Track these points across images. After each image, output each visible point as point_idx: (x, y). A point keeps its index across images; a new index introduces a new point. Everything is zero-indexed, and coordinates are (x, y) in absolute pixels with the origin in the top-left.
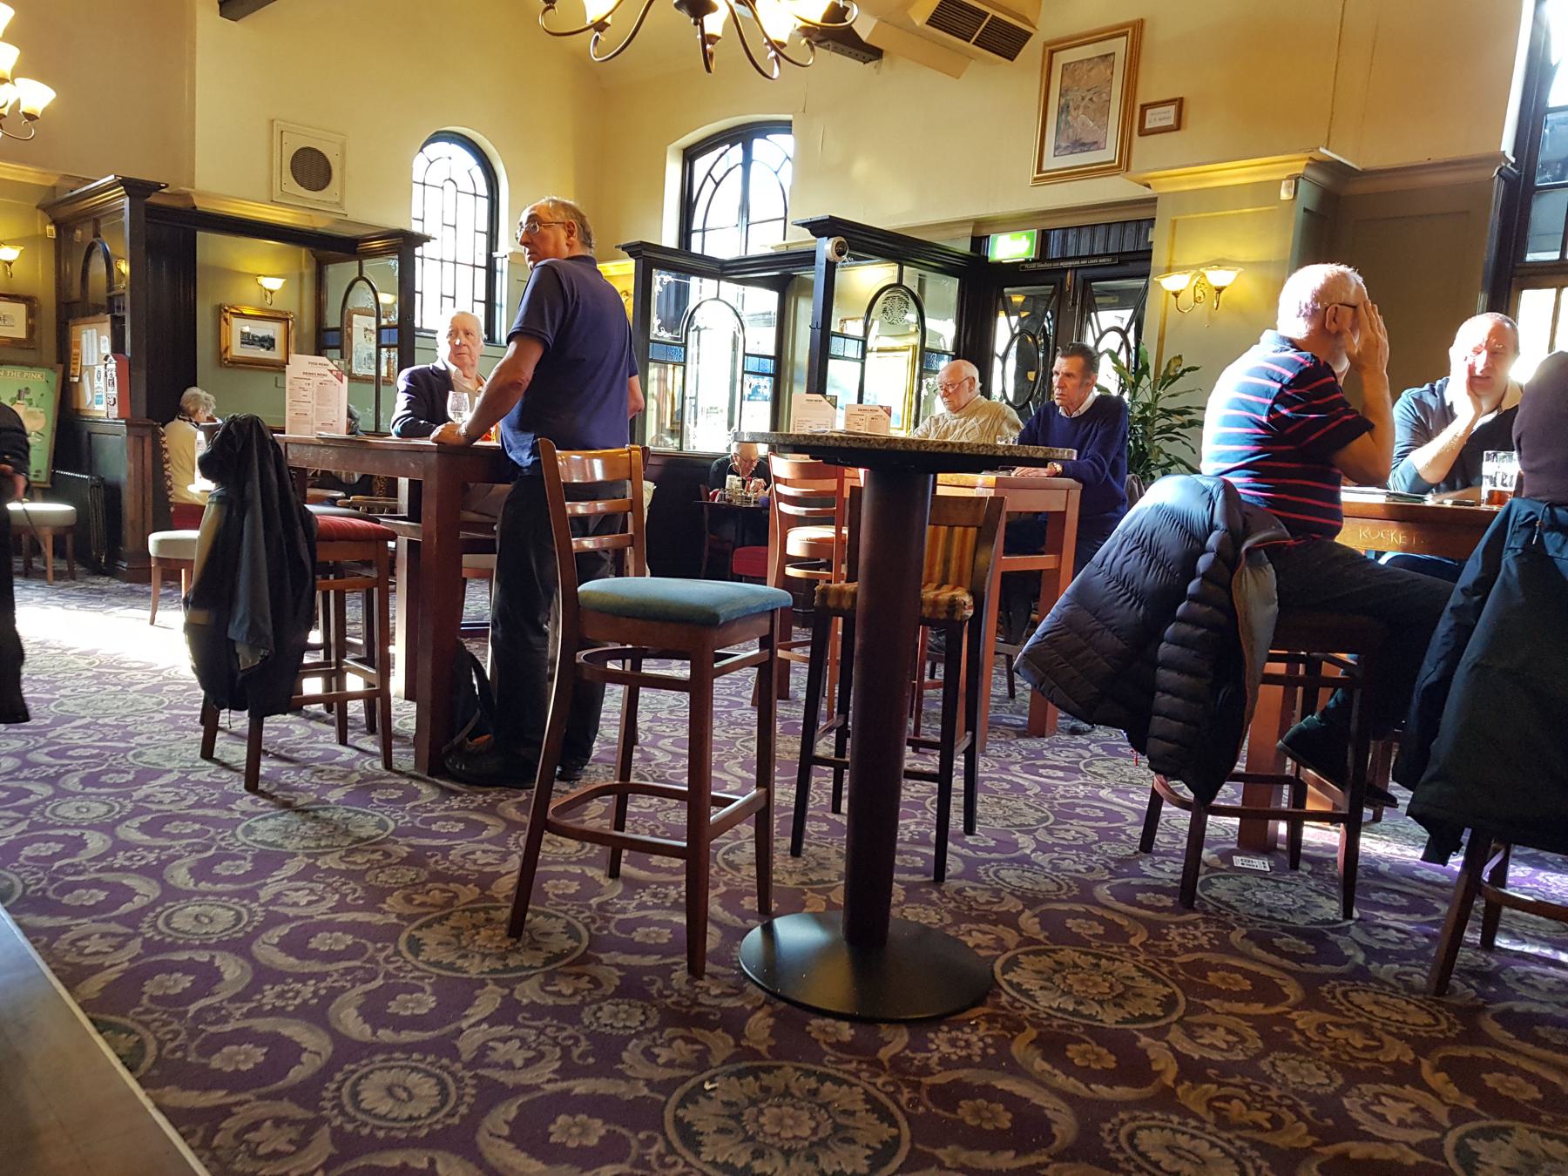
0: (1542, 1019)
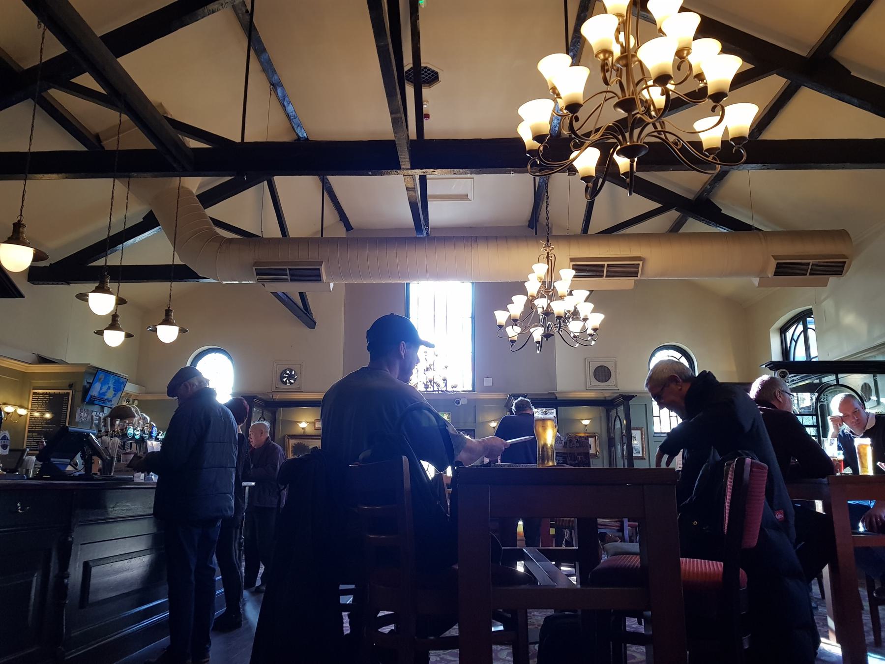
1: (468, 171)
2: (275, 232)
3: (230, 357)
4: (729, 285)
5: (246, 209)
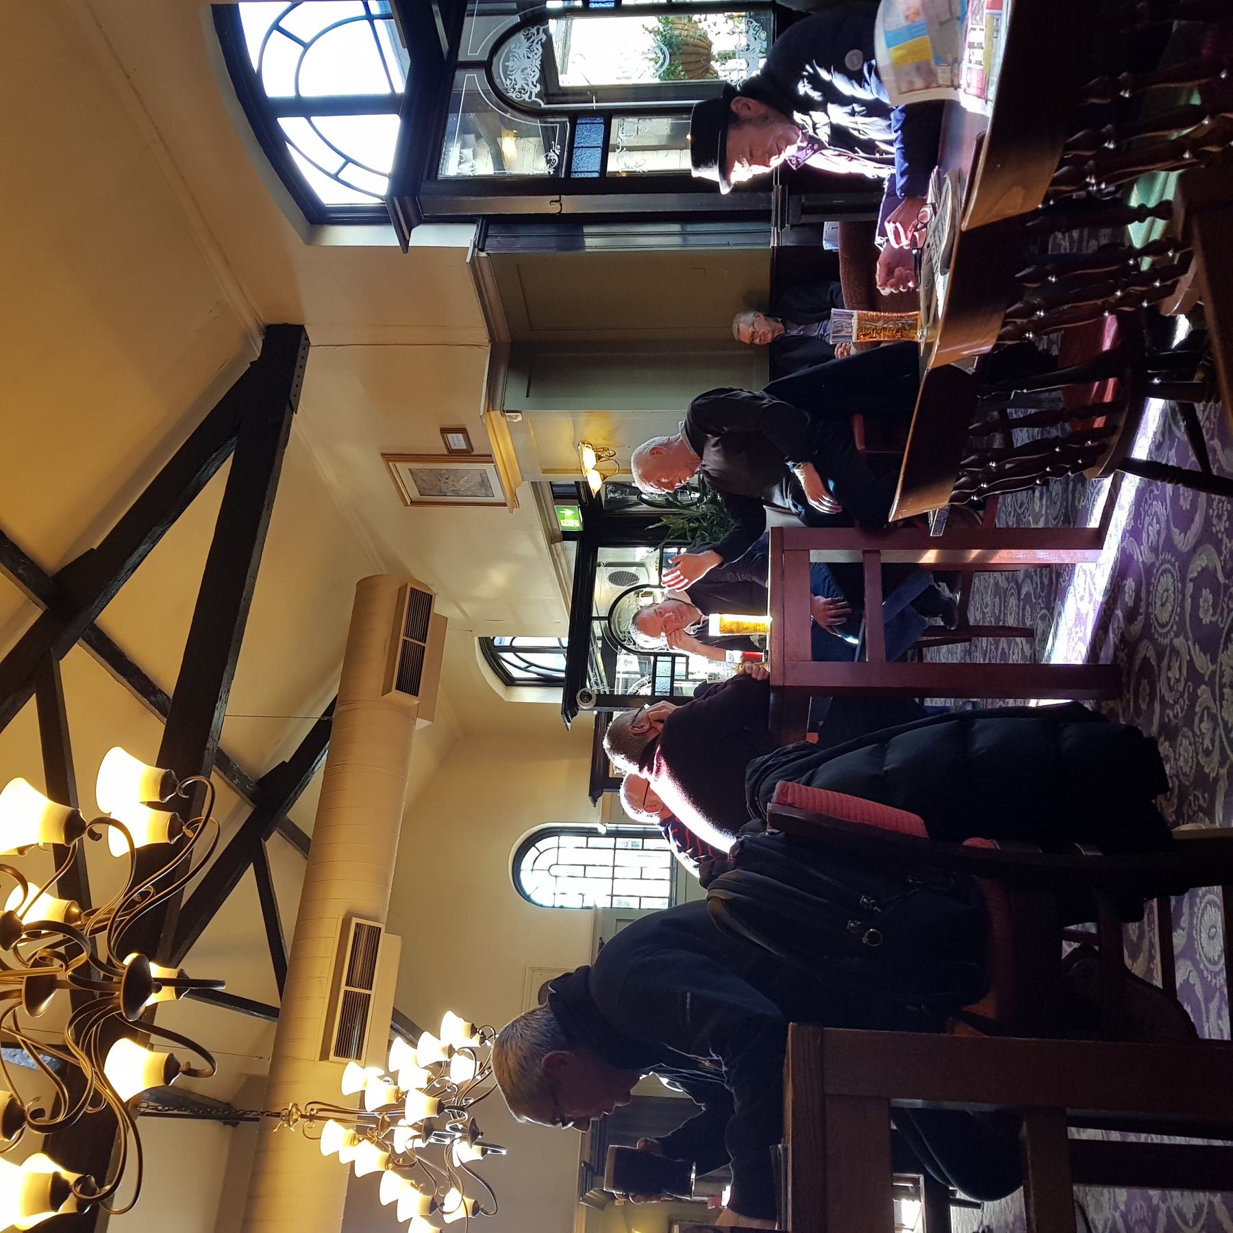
4: (421, 757)
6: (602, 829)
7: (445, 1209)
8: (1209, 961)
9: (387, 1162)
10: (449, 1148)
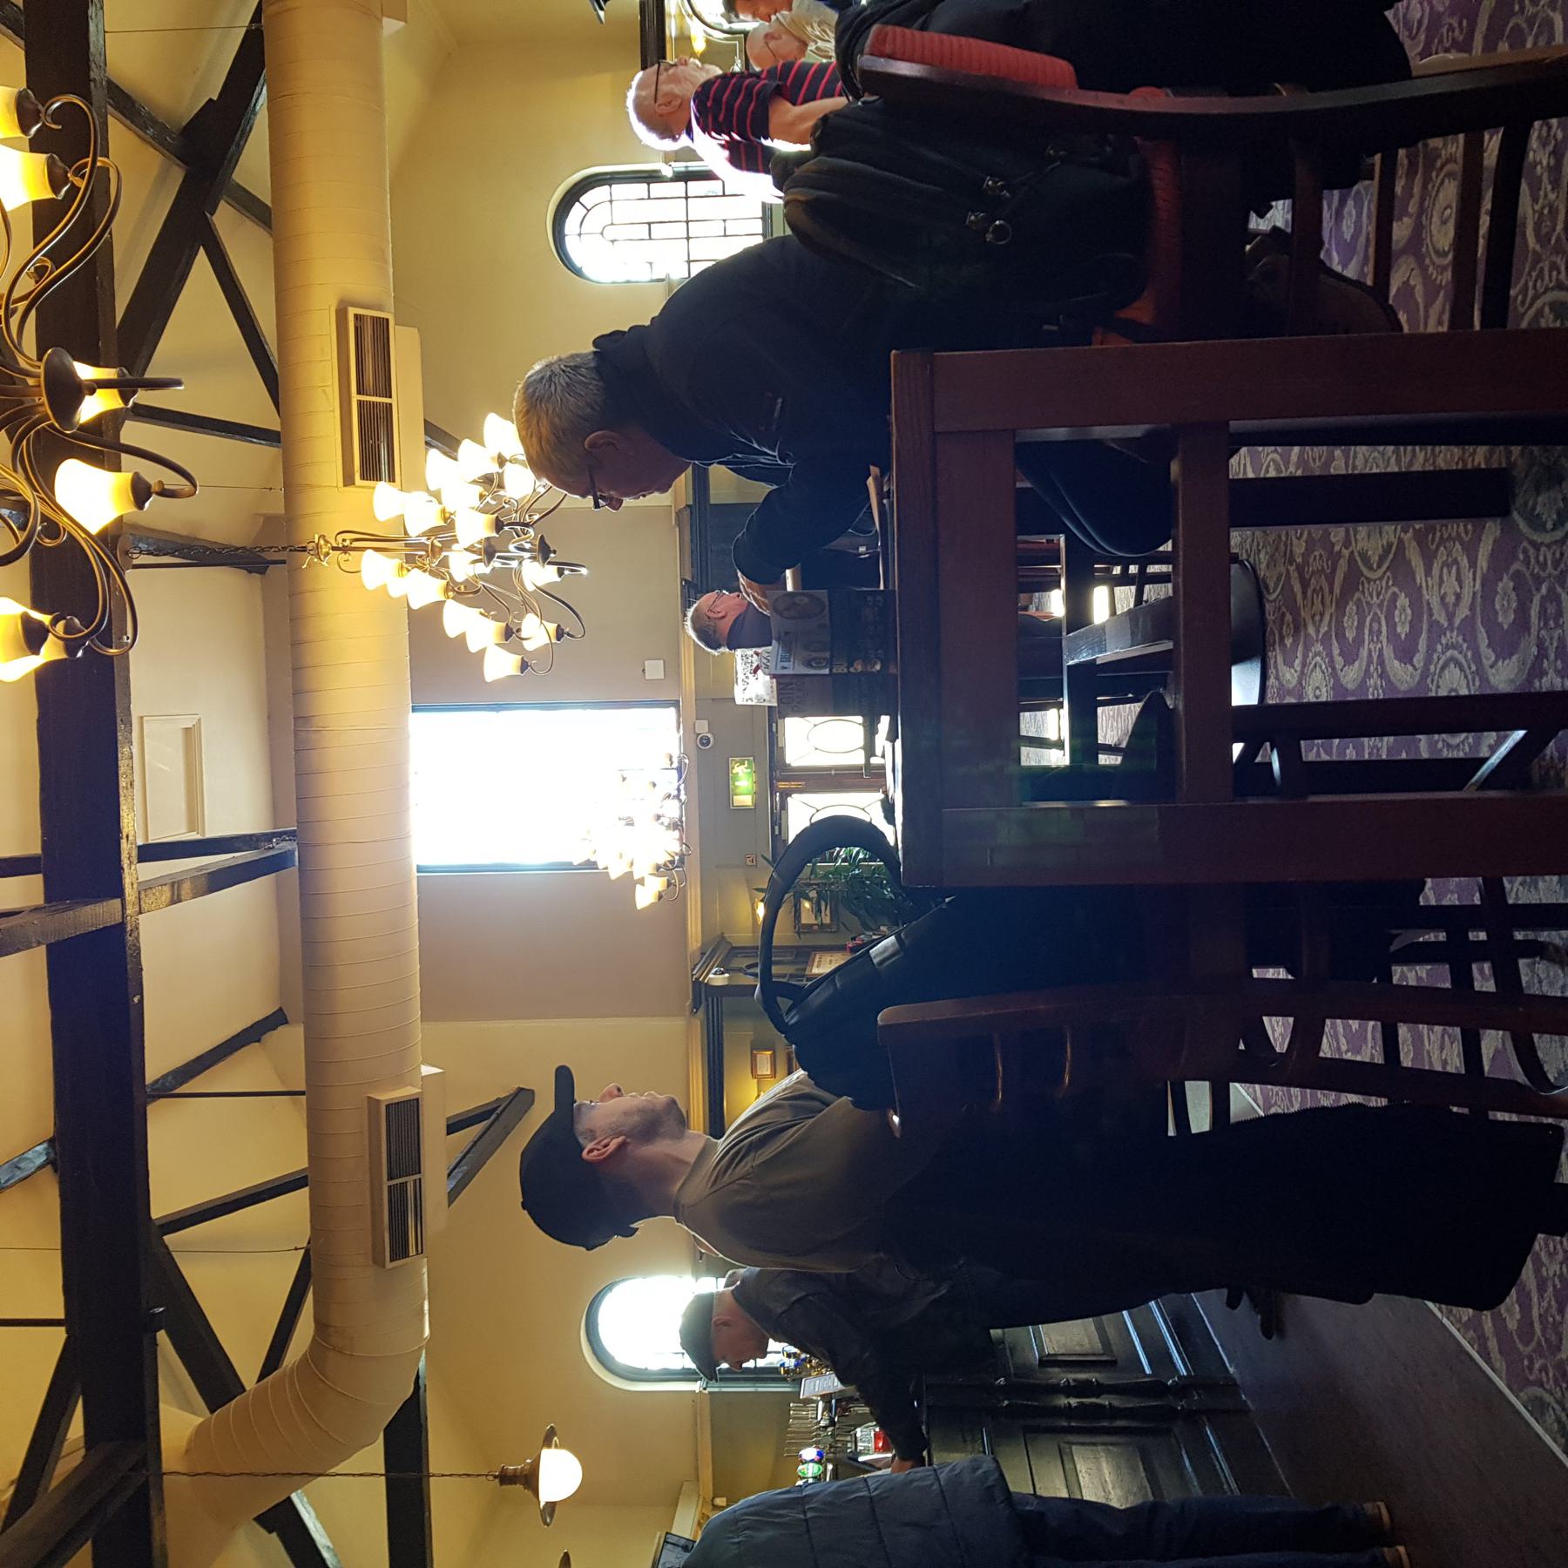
0: (1393, 635)
1: (123, 751)
2: (299, 1199)
3: (610, 1287)
4: (401, 84)
5: (238, 1285)
6: (667, 172)
7: (523, 635)
8: (1437, 252)
9: (446, 590)
10: (519, 573)
